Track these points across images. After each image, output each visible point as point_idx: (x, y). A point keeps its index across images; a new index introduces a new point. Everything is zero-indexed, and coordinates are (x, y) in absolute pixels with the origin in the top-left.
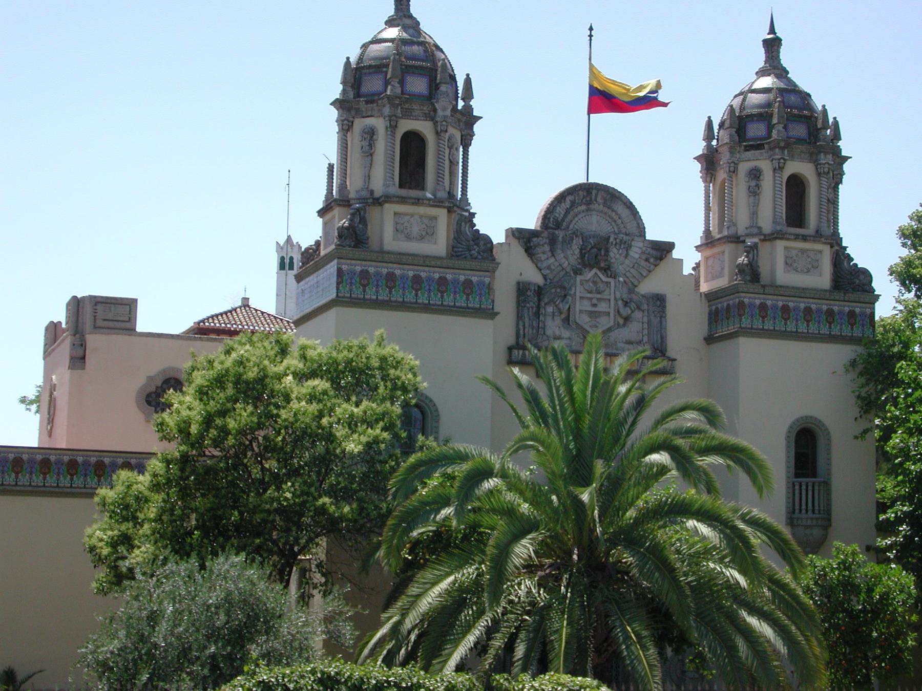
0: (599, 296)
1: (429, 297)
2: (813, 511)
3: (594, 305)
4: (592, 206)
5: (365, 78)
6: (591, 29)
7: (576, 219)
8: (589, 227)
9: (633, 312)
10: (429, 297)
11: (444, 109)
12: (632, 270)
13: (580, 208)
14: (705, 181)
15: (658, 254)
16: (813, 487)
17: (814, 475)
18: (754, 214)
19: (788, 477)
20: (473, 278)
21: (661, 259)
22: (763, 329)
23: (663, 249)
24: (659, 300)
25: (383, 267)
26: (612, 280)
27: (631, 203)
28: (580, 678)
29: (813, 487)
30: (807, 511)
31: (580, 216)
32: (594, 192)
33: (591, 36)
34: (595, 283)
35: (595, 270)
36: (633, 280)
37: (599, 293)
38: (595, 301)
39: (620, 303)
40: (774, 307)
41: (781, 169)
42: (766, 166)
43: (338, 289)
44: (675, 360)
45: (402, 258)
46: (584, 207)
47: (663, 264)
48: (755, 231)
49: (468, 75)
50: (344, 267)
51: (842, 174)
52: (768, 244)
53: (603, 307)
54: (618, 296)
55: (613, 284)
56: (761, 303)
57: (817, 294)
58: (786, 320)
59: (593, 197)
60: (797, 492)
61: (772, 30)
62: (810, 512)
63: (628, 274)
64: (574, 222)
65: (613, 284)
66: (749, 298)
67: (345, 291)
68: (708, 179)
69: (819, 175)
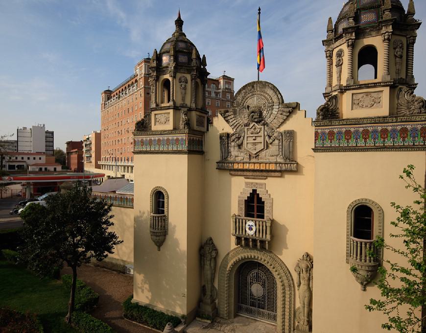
4: (254, 93)
5: (187, 62)
6: (259, 10)
13: (248, 95)
15: (287, 110)
18: (183, 99)
22: (331, 147)
25: (165, 137)
28: (7, 250)
30: (366, 261)
32: (255, 85)
33: (259, 13)
40: (172, 140)
43: (315, 143)
45: (357, 122)
50: (319, 131)
57: (382, 120)
61: (179, 17)
62: (358, 260)
64: (246, 101)
66: (167, 137)
67: (319, 143)
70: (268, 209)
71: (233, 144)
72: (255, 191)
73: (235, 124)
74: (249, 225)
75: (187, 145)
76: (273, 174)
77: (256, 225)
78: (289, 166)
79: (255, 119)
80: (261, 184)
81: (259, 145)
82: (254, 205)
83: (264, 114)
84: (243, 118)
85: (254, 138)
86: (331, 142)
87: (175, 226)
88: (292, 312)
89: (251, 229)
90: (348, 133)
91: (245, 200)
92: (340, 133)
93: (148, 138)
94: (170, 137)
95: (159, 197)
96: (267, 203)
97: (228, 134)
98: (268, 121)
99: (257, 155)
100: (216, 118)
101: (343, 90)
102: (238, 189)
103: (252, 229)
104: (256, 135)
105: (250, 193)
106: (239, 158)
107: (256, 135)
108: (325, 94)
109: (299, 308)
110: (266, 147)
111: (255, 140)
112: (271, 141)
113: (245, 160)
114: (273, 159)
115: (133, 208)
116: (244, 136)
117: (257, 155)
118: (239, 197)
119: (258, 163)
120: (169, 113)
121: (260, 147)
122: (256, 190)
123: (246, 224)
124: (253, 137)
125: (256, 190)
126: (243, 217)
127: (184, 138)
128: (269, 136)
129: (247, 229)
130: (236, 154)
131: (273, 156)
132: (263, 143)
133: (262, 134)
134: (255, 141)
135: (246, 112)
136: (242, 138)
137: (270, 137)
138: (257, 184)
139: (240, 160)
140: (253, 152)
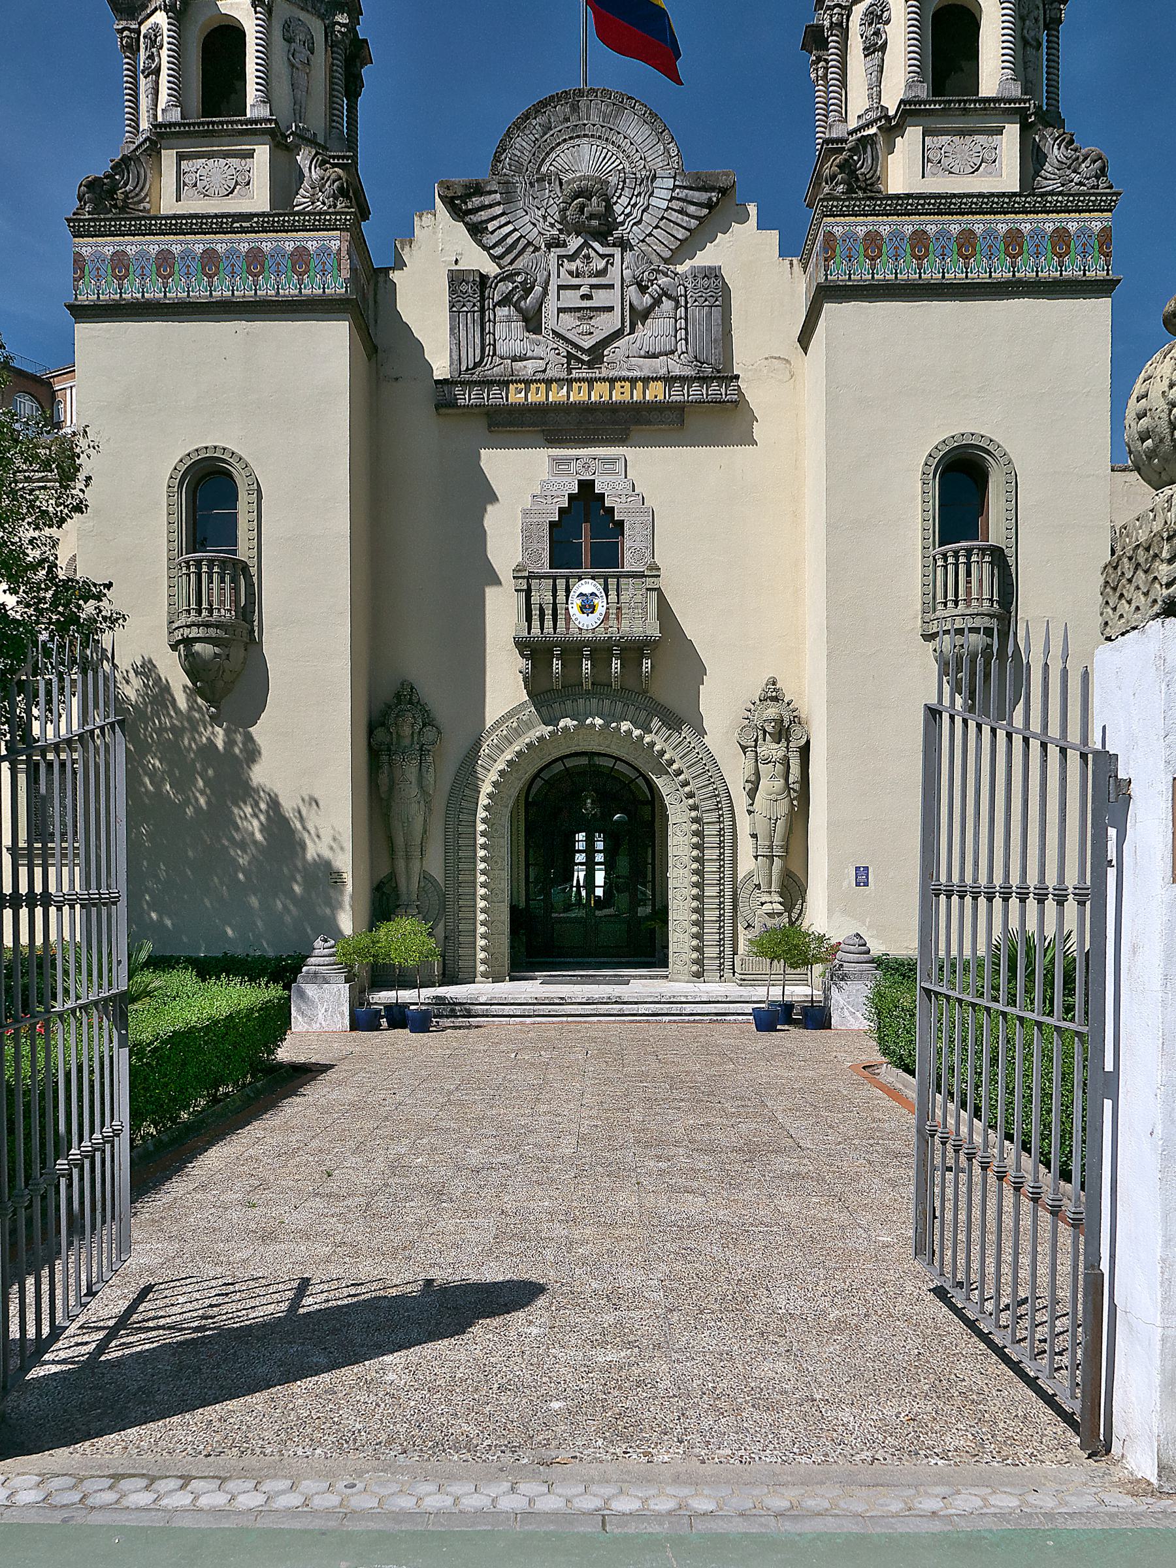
3: (587, 297)
26: (617, 252)
53: (601, 298)
55: (618, 257)
56: (1056, 230)
71: (502, 312)
72: (586, 486)
73: (510, 241)
74: (581, 594)
75: (346, 274)
77: (606, 590)
78: (705, 407)
79: (592, 217)
80: (613, 460)
81: (605, 316)
82: (586, 532)
83: (617, 209)
84: (533, 219)
85: (584, 290)
88: (728, 893)
89: (588, 607)
91: (552, 524)
92: (187, 255)
93: (132, 246)
94: (267, 243)
95: (210, 494)
96: (632, 528)
97: (484, 278)
98: (634, 234)
99: (596, 354)
100: (427, 219)
102: (524, 483)
103: (593, 609)
104: (594, 281)
105: (571, 497)
106: (529, 364)
107: (594, 281)
108: (909, 102)
109: (750, 875)
110: (627, 324)
111: (587, 297)
112: (647, 300)
113: (550, 374)
114: (659, 366)
116: (547, 283)
117: (596, 354)
118: (526, 513)
119: (604, 380)
120: (250, 155)
121: (607, 324)
123: (568, 591)
124: (578, 287)
127: (335, 245)
128: (639, 284)
129: (574, 610)
130: (517, 348)
131: (654, 356)
132: (618, 309)
133: (614, 275)
135: (553, 201)
136: (538, 289)
137: (643, 289)
139: (530, 371)
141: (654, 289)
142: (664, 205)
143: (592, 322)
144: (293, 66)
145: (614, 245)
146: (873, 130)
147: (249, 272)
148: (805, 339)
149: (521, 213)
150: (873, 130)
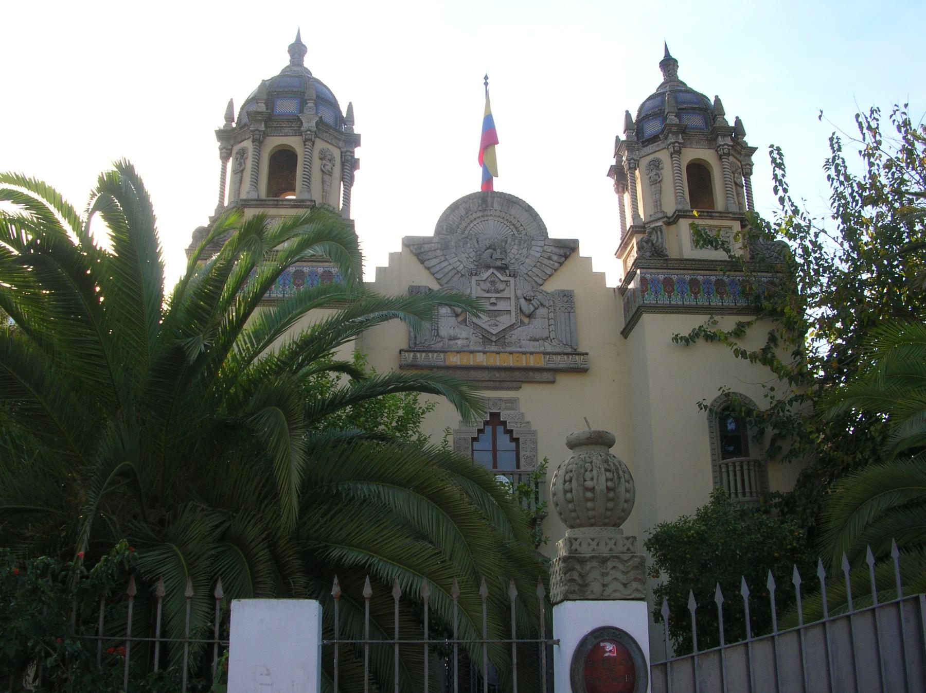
0: (498, 295)
1: (284, 291)
2: (744, 494)
3: (494, 304)
4: (488, 213)
7: (472, 225)
8: (493, 236)
9: (536, 309)
10: (284, 291)
11: (309, 121)
12: (534, 269)
14: (617, 192)
15: (562, 252)
16: (742, 467)
17: (748, 456)
19: (713, 460)
20: (333, 270)
21: (566, 257)
23: (568, 248)
24: (568, 297)
26: (512, 280)
27: (530, 207)
29: (742, 467)
30: (744, 495)
31: (475, 222)
33: (486, 84)
34: (493, 283)
35: (491, 271)
36: (537, 279)
37: (498, 292)
38: (493, 300)
39: (522, 301)
41: (678, 152)
42: (664, 156)
44: (587, 354)
46: (479, 214)
47: (569, 265)
48: (660, 215)
49: (350, 103)
51: (751, 165)
52: (673, 227)
53: (502, 305)
54: (519, 295)
55: (512, 283)
56: (665, 278)
58: (696, 294)
59: (489, 204)
60: (731, 474)
62: (740, 495)
63: (530, 273)
65: (512, 283)
68: (620, 189)
69: (720, 158)
70: (528, 454)
76: (538, 376)
80: (508, 401)
86: (670, 297)
87: (717, 100)
90: (694, 283)
92: (681, 281)
101: (672, 221)
104: (498, 295)
106: (459, 342)
108: (679, 211)
111: (494, 304)
115: (582, 371)
122: (499, 414)
125: (499, 414)
126: (639, 525)
134: (495, 308)
138: (500, 399)
140: (492, 331)
141: (535, 303)
142: (539, 255)
143: (498, 319)
144: (323, 171)
145: (510, 275)
146: (660, 223)
147: (295, 284)
148: (585, 418)
149: (453, 255)
150: (660, 223)
